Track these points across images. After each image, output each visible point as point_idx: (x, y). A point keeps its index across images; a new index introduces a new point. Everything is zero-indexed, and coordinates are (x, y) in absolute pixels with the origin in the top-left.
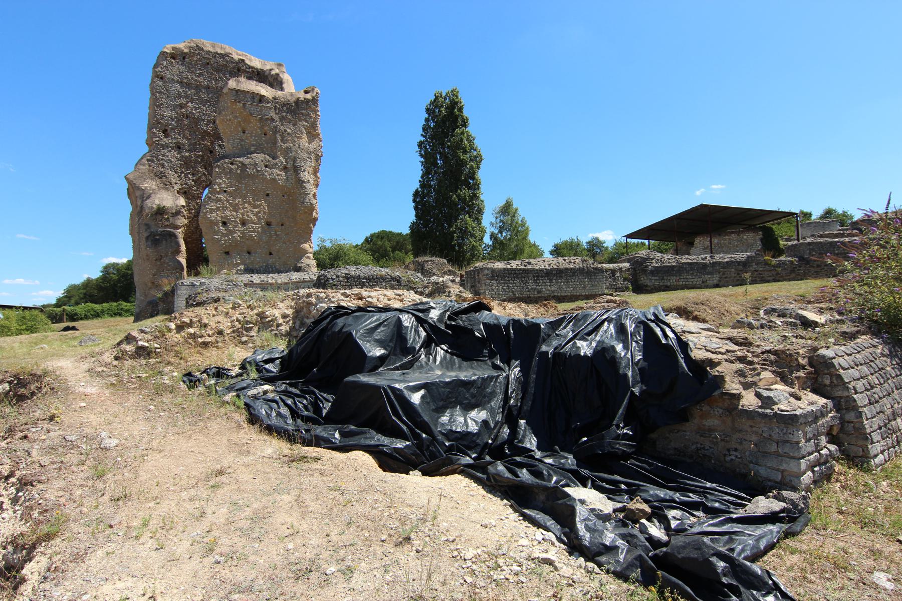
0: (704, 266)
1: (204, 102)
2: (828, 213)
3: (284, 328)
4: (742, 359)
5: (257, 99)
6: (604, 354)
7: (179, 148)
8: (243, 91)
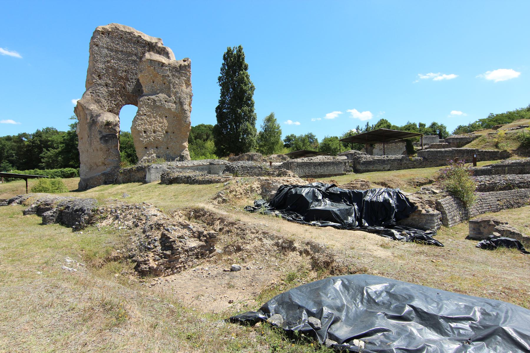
0: (384, 161)
1: (120, 60)
2: (434, 125)
3: (259, 192)
4: (421, 202)
5: (161, 65)
6: (386, 201)
7: (107, 85)
8: (154, 60)
